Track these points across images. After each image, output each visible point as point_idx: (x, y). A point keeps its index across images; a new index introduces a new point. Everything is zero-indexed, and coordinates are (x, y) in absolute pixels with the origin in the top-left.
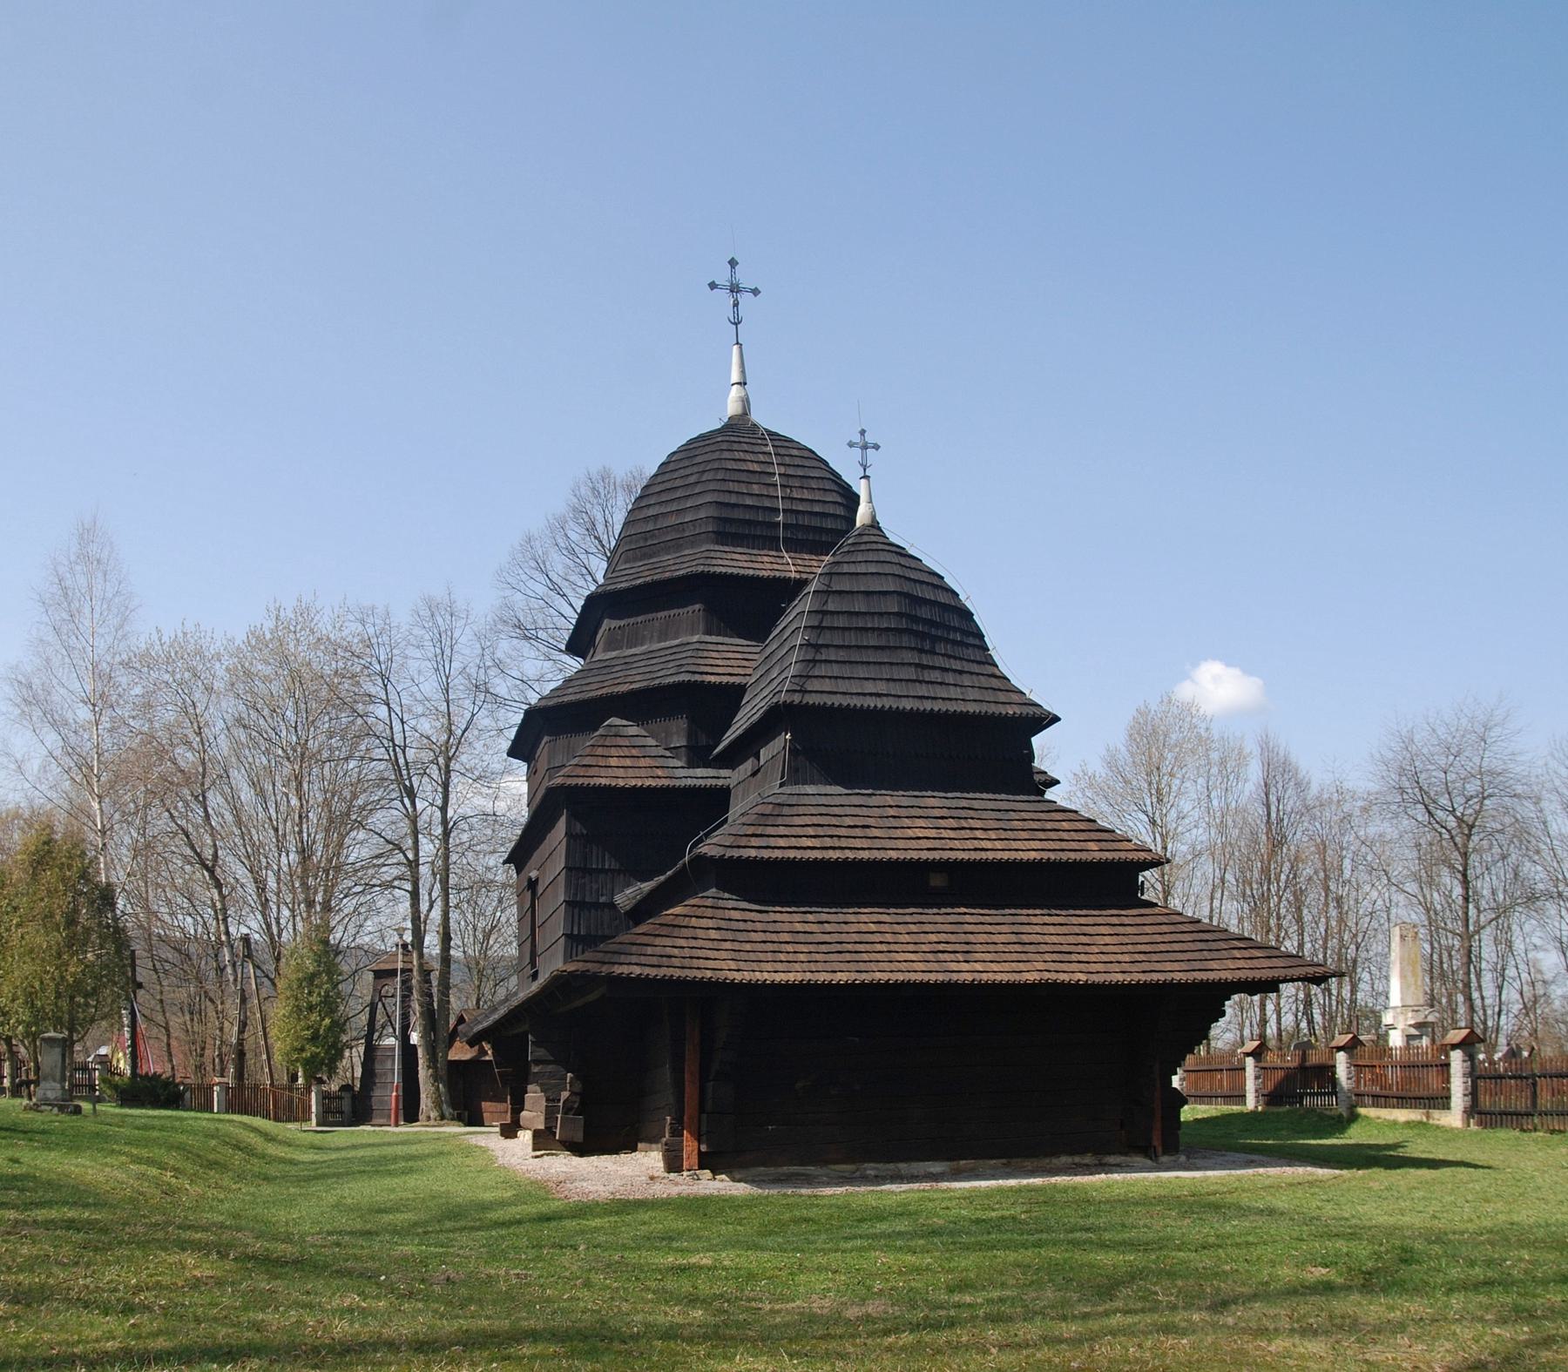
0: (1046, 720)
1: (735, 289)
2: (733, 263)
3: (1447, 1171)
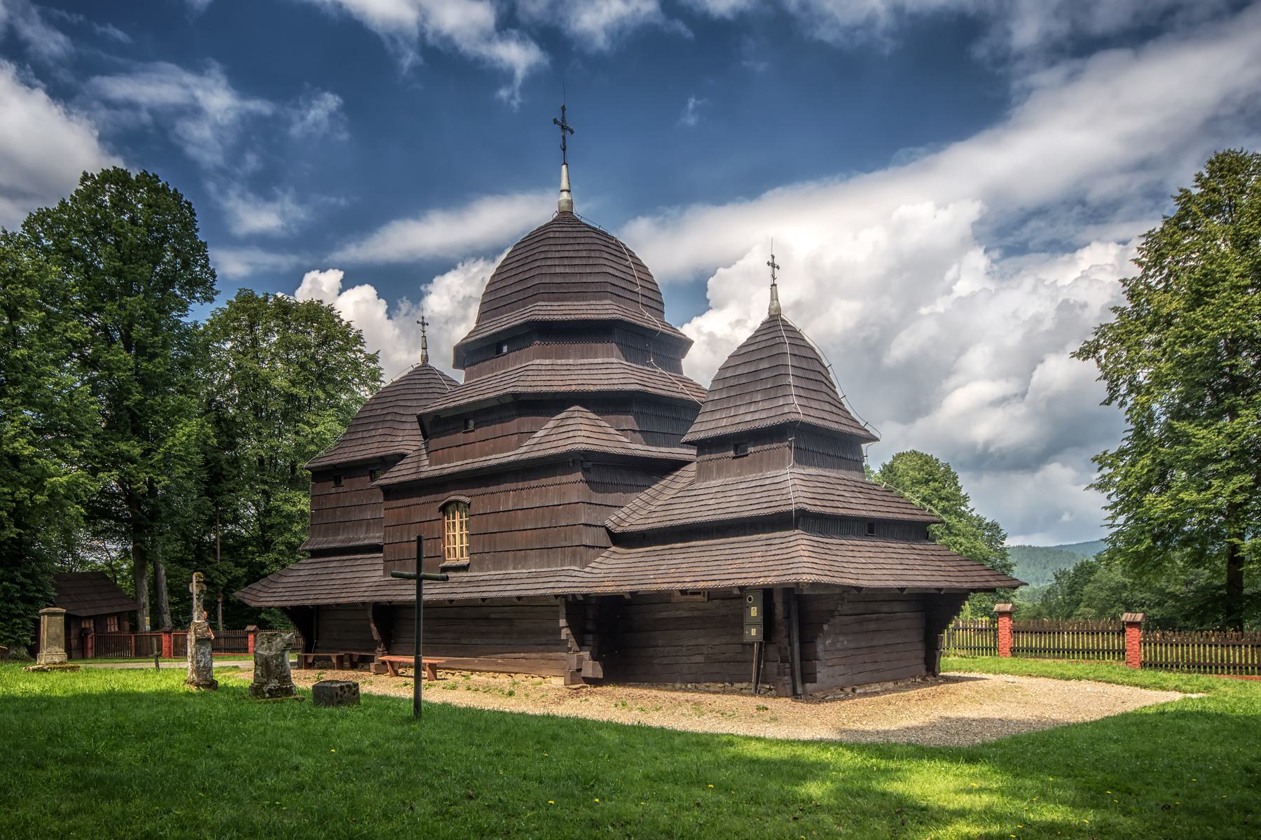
0: (875, 439)
1: (564, 128)
2: (563, 109)
3: (970, 683)
